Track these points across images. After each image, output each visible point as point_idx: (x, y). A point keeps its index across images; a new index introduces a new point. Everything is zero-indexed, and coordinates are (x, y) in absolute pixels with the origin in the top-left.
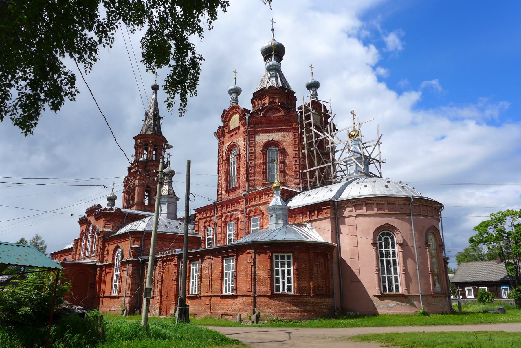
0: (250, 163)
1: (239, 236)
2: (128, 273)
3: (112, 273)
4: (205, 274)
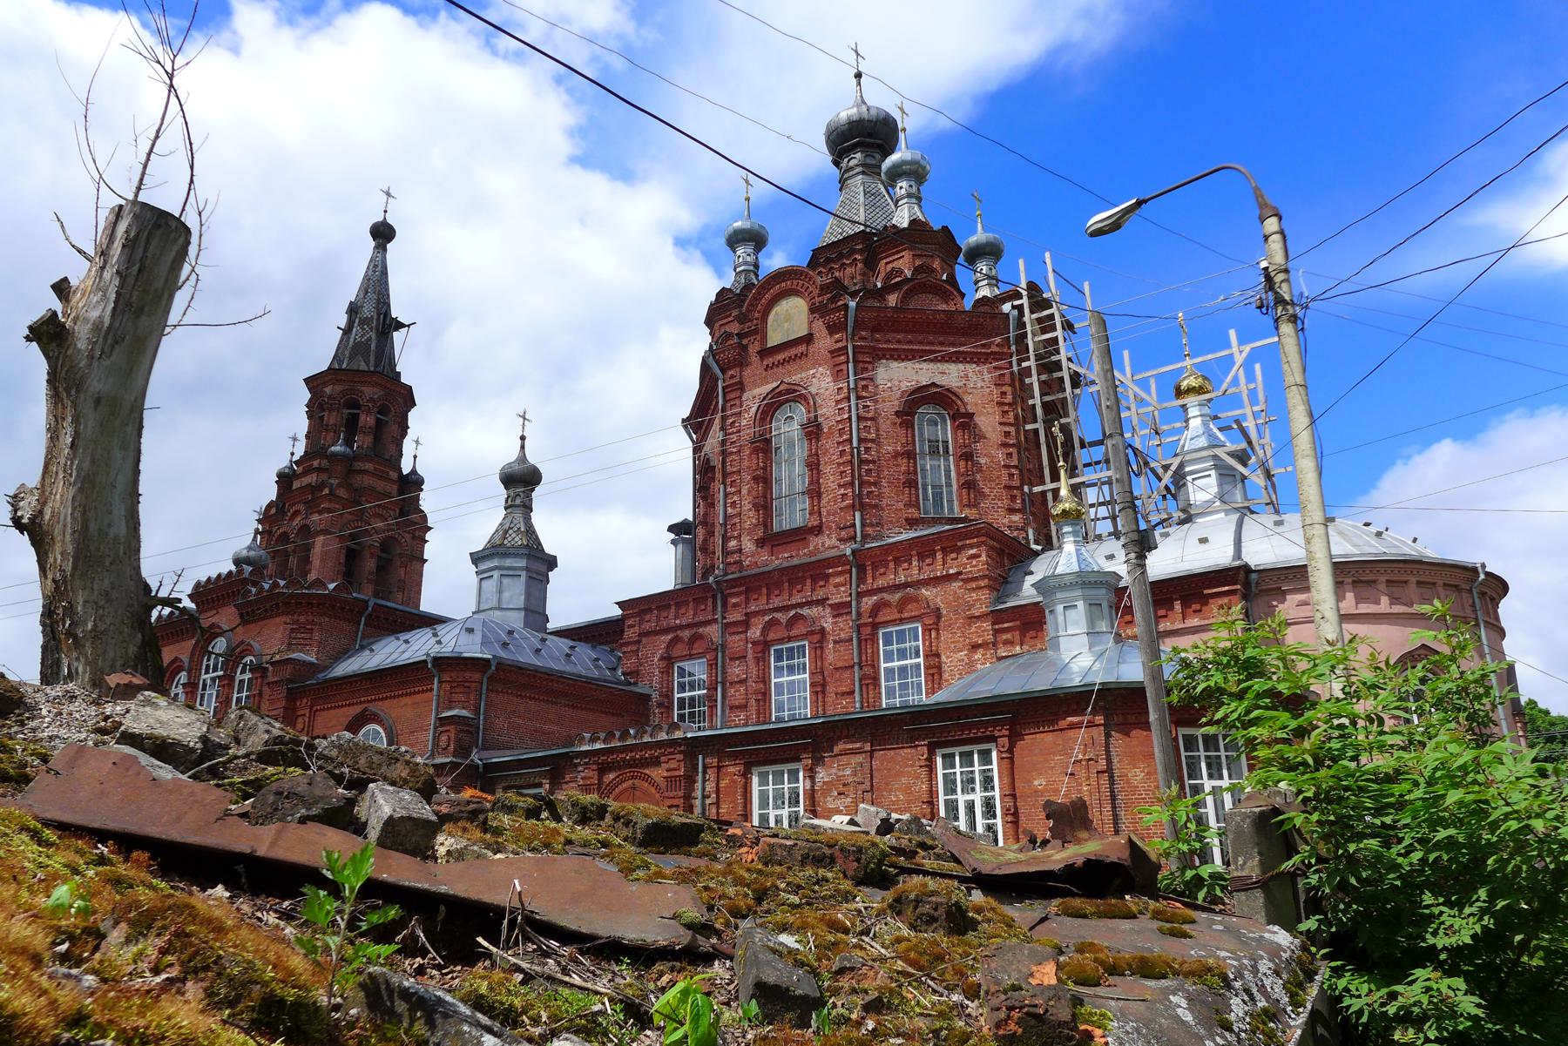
1: (830, 689)
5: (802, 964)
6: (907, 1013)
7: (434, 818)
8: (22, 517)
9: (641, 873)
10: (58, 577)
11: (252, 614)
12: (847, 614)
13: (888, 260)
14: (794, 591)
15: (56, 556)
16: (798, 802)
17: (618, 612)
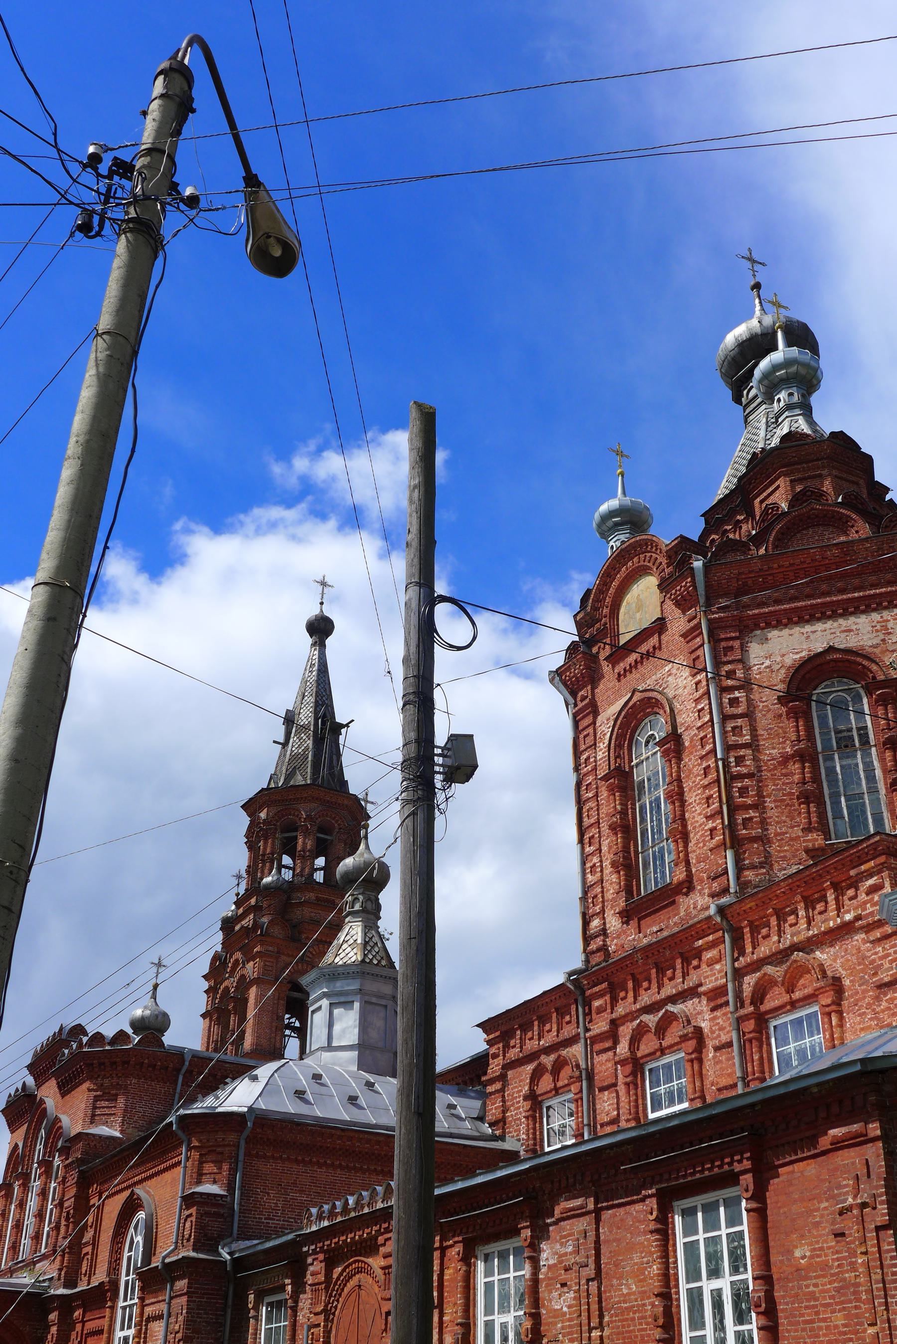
0: (732, 760)
2: (171, 1326)
3: (105, 1335)
4: (559, 1314)
13: (762, 497)
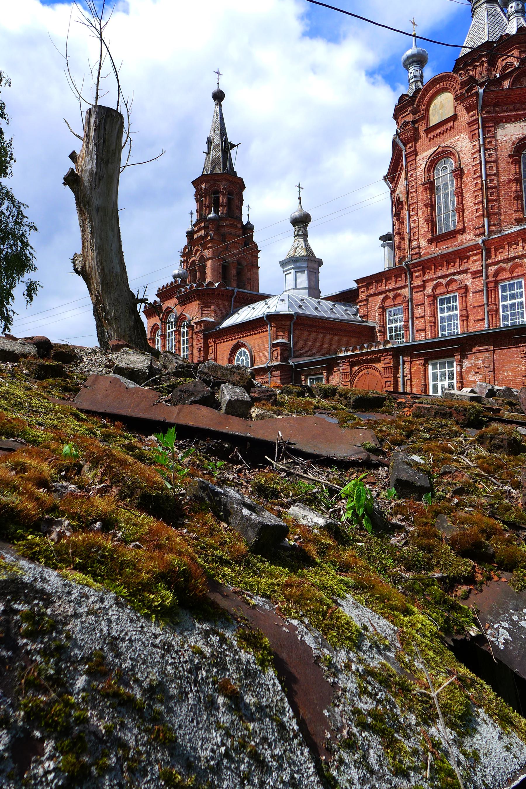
1: (471, 318)
5: (422, 470)
6: (477, 495)
7: (249, 400)
8: (78, 268)
9: (349, 423)
10: (97, 294)
11: (184, 301)
12: (480, 277)
14: (450, 267)
15: (94, 285)
16: (453, 378)
17: (355, 286)
